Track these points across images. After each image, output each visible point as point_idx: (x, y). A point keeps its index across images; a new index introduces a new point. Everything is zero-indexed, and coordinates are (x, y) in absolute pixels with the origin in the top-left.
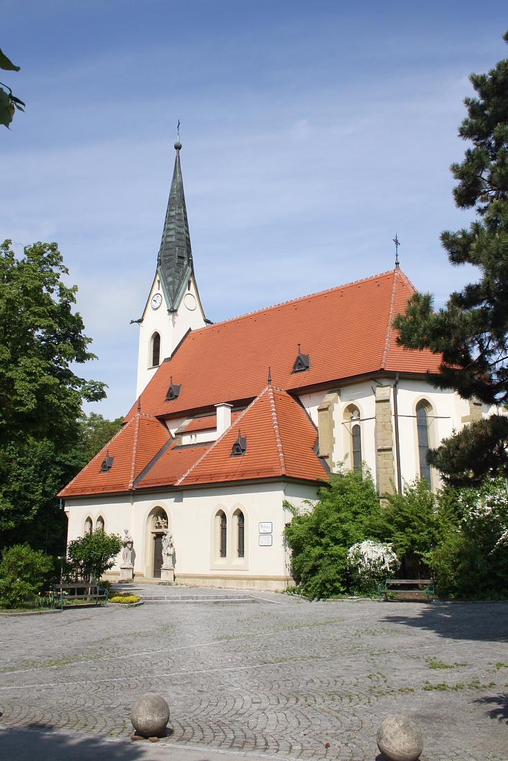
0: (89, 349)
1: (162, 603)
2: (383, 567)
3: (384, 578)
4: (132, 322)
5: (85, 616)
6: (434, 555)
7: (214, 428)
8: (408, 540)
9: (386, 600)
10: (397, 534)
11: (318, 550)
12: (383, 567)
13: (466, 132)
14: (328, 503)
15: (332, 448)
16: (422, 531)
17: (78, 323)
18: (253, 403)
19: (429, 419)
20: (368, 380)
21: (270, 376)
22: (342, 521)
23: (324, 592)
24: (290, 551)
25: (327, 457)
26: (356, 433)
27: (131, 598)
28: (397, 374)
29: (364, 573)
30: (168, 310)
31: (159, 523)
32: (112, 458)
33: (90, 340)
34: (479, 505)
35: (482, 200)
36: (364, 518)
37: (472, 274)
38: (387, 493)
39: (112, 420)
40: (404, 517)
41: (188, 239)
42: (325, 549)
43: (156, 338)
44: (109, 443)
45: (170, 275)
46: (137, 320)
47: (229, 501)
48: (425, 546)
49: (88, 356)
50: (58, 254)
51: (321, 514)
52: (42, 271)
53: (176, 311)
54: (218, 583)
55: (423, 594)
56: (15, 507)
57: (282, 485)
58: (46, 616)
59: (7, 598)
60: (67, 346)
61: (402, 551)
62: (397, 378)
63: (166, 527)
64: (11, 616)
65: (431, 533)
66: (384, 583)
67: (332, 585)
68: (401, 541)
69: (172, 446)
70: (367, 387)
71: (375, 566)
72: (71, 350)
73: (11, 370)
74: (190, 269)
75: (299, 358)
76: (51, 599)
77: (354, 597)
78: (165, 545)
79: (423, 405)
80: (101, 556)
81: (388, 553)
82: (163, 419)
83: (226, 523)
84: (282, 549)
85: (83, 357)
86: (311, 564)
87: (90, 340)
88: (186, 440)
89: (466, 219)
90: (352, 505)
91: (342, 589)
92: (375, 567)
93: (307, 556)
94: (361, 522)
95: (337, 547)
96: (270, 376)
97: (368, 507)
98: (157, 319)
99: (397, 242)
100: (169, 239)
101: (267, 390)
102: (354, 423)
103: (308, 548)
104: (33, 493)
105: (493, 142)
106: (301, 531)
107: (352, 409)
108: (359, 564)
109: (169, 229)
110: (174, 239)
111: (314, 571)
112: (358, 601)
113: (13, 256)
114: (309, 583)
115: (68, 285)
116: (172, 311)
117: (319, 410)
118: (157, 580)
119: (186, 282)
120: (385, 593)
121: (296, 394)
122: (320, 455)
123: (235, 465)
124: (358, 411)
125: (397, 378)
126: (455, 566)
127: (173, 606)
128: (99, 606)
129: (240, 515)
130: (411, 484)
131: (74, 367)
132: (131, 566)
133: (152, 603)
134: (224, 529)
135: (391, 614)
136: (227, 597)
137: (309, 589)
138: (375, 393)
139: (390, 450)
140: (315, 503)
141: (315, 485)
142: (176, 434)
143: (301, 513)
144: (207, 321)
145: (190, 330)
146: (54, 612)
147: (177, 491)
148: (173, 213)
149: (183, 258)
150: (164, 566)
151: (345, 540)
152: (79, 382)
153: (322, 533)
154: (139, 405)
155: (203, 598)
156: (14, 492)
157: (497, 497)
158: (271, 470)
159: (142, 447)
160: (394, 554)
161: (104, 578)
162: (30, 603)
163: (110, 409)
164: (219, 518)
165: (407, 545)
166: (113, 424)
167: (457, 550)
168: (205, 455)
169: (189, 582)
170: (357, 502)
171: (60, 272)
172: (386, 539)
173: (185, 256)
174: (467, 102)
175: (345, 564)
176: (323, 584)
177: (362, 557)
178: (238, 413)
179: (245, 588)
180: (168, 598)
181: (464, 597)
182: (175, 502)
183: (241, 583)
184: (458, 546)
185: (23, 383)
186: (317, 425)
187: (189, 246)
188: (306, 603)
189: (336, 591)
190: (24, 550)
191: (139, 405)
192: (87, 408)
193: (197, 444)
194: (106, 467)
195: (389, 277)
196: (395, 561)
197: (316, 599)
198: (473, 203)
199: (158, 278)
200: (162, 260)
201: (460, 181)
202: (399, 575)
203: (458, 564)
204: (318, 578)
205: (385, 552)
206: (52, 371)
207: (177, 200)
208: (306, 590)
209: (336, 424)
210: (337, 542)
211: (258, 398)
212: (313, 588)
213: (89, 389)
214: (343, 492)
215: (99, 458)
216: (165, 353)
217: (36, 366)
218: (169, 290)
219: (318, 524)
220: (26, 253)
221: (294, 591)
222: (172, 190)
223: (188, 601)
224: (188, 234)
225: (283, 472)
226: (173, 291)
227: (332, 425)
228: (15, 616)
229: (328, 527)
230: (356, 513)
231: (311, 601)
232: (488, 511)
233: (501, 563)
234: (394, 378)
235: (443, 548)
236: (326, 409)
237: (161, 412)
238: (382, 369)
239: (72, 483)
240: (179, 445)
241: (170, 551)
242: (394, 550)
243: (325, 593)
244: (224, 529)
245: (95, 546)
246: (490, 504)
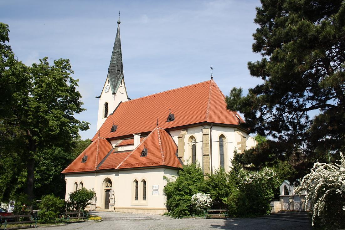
0: (82, 107)
1: (111, 220)
2: (206, 204)
3: (207, 209)
4: (96, 97)
5: (79, 227)
6: (227, 199)
7: (133, 144)
8: (217, 193)
9: (207, 218)
10: (212, 190)
11: (178, 197)
12: (206, 204)
13: (256, 21)
14: (182, 177)
15: (184, 154)
16: (222, 189)
17: (78, 95)
18: (150, 134)
19: (224, 143)
20: (199, 126)
21: (157, 123)
22: (189, 185)
23: (181, 215)
24: (166, 197)
25: (182, 158)
26: (194, 148)
27: (98, 218)
28: (212, 124)
29: (198, 207)
31: (108, 185)
32: (87, 156)
33: (82, 103)
34: (247, 178)
35: (264, 50)
36: (197, 184)
37: (259, 81)
38: (208, 174)
39: (84, 140)
40: (215, 183)
41: (122, 63)
42: (182, 196)
43: (107, 105)
44: (85, 150)
46: (98, 97)
47: (140, 176)
48: (223, 196)
49: (83, 110)
50: (69, 65)
51: (180, 182)
52: (62, 72)
53: (115, 93)
54: (134, 211)
55: (223, 215)
56: (42, 177)
57: (163, 169)
58: (61, 227)
59: (43, 219)
60: (72, 105)
61: (214, 197)
62: (212, 125)
63: (111, 187)
64: (46, 227)
65: (226, 190)
66: (206, 211)
67: (184, 212)
68: (214, 194)
69: (113, 152)
70: (199, 128)
71: (202, 204)
72: (75, 107)
73: (47, 115)
74: (122, 76)
75: (170, 115)
76: (62, 219)
77: (194, 217)
78: (110, 194)
79: (222, 137)
80: (85, 200)
81: (208, 198)
82: (109, 140)
83: (138, 185)
84: (163, 196)
85: (79, 110)
86: (175, 203)
87: (82, 103)
88: (120, 149)
89: (257, 58)
90: (193, 178)
91: (188, 214)
92: (203, 204)
93: (173, 200)
94: (197, 185)
95: (186, 196)
96: (157, 123)
97: (199, 179)
98: (107, 97)
99: (212, 68)
100: (113, 62)
101: (156, 128)
102: (193, 144)
103: (174, 196)
104: (50, 171)
105: (268, 26)
106: (171, 189)
107: (192, 137)
108: (196, 203)
109: (114, 58)
110: (115, 62)
111: (177, 206)
112: (195, 219)
113: (48, 64)
114: (174, 211)
115: (75, 79)
116: (114, 93)
117: (178, 138)
118: (107, 210)
119: (120, 81)
120: (207, 215)
121: (168, 131)
122: (178, 157)
123: (142, 160)
124: (195, 138)
125: (212, 125)
126: (236, 204)
127: (117, 222)
128: (84, 222)
129: (144, 182)
130: (217, 169)
131: (76, 116)
132: (95, 204)
133: (107, 220)
134: (137, 188)
135: (213, 224)
136: (139, 217)
137: (175, 214)
138: (202, 131)
139: (209, 155)
140: (177, 177)
141: (177, 170)
142: (115, 147)
143: (171, 181)
144: (129, 99)
145: (121, 102)
146: (65, 225)
147: (116, 171)
148: (116, 51)
149: (119, 71)
150: (110, 204)
151: (190, 193)
152: (77, 122)
153: (180, 190)
154: (99, 133)
155: (129, 218)
156: (42, 171)
157: (254, 175)
158: (159, 162)
159: (100, 152)
160: (211, 199)
161: (86, 209)
162: (52, 221)
163: (84, 136)
164: (135, 183)
165: (216, 195)
166: (85, 142)
167: (238, 197)
168: (129, 156)
169: (121, 210)
170: (195, 177)
171: (70, 73)
172: (207, 192)
173: (120, 70)
174: (257, 9)
175: (190, 203)
176: (181, 212)
177: (197, 200)
178: (143, 138)
179: (146, 213)
180: (114, 218)
181: (240, 216)
182: (115, 176)
183: (145, 212)
184: (237, 195)
185: (53, 121)
186: (177, 144)
187: (122, 66)
188: (173, 219)
189: (186, 215)
190: (51, 197)
191: (99, 133)
192: (80, 133)
194: (84, 160)
195: (208, 83)
196: (211, 202)
197: (177, 218)
198: (260, 51)
199: (108, 79)
200: (110, 71)
201: (256, 41)
202: (213, 208)
203: (238, 203)
204: (177, 209)
205: (207, 198)
206: (65, 116)
207: (118, 46)
208: (173, 214)
209: (185, 144)
210: (186, 193)
211: (152, 132)
212: (176, 213)
213: (82, 125)
214: (189, 172)
215: (81, 156)
216: (110, 111)
217: (59, 114)
218: (113, 84)
219: (179, 186)
220: (55, 63)
221: (168, 214)
222: (116, 41)
223: (123, 219)
225: (164, 163)
226: (115, 84)
227: (184, 144)
228: (47, 227)
229: (183, 187)
230: (194, 182)
231: (175, 219)
232: (250, 181)
233: (255, 203)
234: (211, 125)
235: (231, 196)
236: (182, 137)
237: (109, 137)
238: (206, 121)
239: (68, 167)
241: (113, 197)
242: (211, 197)
243: (181, 215)
244: (137, 188)
245: (83, 195)
246: (251, 178)
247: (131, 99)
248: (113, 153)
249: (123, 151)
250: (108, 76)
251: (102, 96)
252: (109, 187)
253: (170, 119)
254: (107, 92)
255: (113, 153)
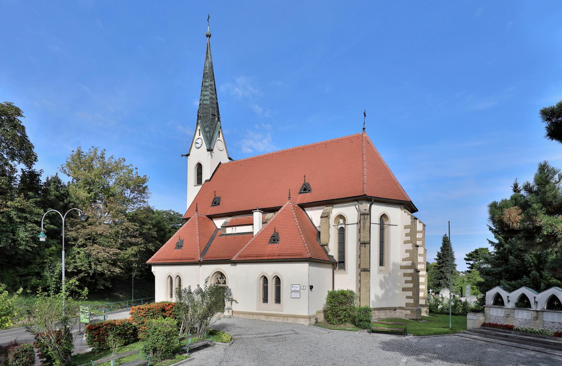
4: (182, 156)
18: (280, 211)
19: (385, 226)
26: (342, 232)
30: (207, 149)
32: (183, 240)
41: (217, 104)
43: (199, 167)
45: (207, 127)
47: (270, 270)
62: (373, 201)
63: (225, 283)
74: (220, 123)
75: (304, 184)
79: (384, 217)
88: (229, 231)
99: (365, 114)
100: (205, 102)
102: (339, 226)
110: (208, 102)
121: (303, 206)
122: (321, 244)
123: (273, 249)
125: (373, 201)
129: (278, 280)
145: (220, 163)
148: (207, 84)
193: (237, 233)
195: (360, 138)
199: (199, 128)
200: (201, 116)
216: (206, 176)
218: (207, 136)
224: (217, 100)
226: (210, 137)
240: (225, 233)
247: (232, 159)
248: (220, 236)
249: (234, 234)
250: (198, 123)
251: (191, 153)
252: (220, 283)
253: (305, 190)
254: (198, 148)
255: (220, 236)
